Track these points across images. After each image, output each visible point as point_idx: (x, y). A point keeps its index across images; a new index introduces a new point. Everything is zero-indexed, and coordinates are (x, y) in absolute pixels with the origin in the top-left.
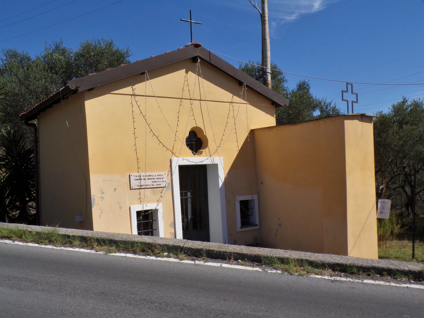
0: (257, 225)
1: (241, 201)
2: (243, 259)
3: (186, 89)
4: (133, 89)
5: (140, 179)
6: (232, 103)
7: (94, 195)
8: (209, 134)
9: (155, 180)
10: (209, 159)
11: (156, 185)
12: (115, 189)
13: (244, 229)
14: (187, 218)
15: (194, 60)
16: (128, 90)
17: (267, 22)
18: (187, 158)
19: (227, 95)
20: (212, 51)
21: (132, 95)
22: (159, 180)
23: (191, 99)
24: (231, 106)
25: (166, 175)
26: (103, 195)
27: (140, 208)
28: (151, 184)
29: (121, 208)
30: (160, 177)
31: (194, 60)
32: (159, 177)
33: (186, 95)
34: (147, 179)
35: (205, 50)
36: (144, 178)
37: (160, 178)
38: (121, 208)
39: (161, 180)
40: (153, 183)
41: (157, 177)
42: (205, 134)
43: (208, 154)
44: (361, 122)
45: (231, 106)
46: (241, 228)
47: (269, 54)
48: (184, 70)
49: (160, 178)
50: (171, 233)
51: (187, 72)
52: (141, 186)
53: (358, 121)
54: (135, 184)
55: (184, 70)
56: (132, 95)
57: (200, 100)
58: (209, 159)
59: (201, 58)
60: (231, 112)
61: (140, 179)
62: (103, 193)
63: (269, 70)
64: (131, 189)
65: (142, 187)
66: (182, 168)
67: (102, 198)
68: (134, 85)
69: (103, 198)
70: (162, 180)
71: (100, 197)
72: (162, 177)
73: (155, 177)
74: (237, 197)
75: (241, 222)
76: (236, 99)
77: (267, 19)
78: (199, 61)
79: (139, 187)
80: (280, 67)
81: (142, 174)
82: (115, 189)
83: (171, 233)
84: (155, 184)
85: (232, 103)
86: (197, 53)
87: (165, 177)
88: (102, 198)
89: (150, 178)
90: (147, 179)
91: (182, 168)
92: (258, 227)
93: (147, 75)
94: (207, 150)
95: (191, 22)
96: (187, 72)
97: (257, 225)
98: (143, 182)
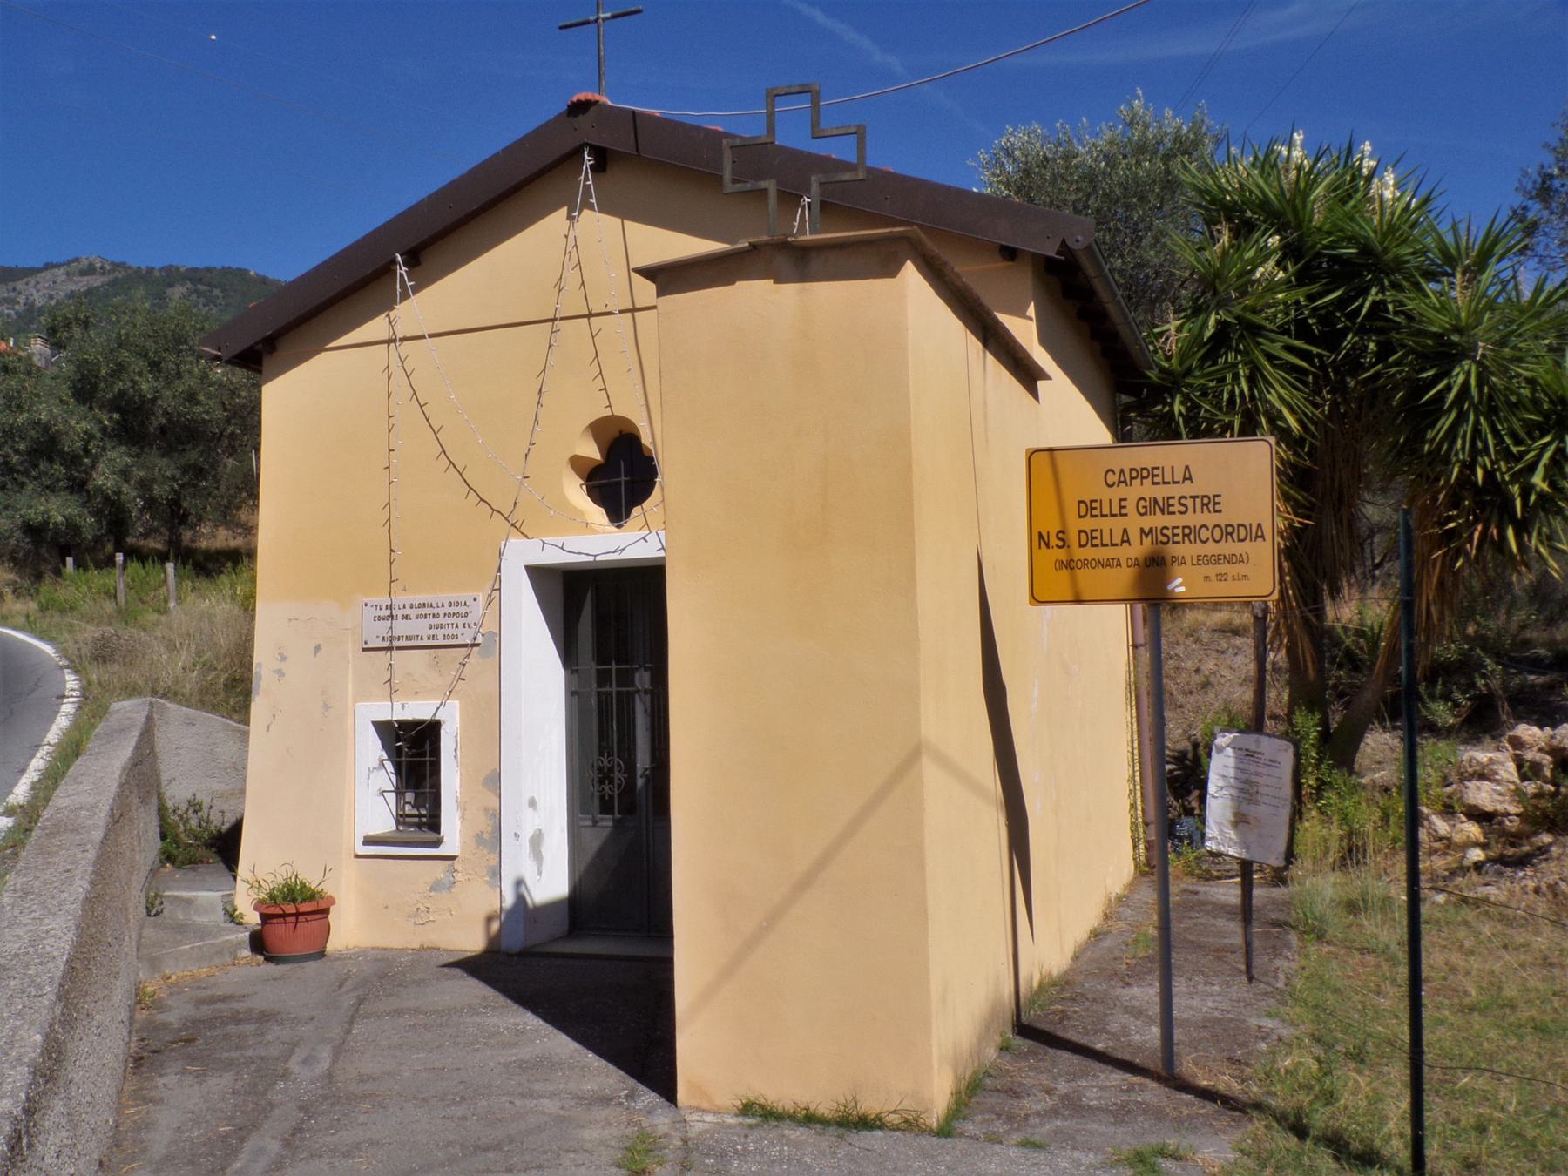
3: (572, 279)
7: (259, 665)
10: (652, 538)
12: (318, 648)
14: (630, 768)
16: (375, 328)
18: (558, 541)
21: (388, 342)
22: (454, 620)
23: (590, 315)
26: (283, 666)
29: (327, 707)
30: (458, 611)
32: (454, 610)
33: (573, 303)
36: (405, 612)
38: (327, 707)
39: (460, 621)
41: (447, 610)
50: (486, 810)
52: (392, 639)
54: (376, 632)
56: (388, 342)
58: (652, 538)
62: (284, 658)
65: (396, 644)
67: (280, 673)
72: (462, 610)
73: (441, 611)
79: (386, 644)
81: (399, 599)
82: (318, 648)
84: (440, 633)
88: (280, 673)
89: (423, 610)
98: (401, 628)
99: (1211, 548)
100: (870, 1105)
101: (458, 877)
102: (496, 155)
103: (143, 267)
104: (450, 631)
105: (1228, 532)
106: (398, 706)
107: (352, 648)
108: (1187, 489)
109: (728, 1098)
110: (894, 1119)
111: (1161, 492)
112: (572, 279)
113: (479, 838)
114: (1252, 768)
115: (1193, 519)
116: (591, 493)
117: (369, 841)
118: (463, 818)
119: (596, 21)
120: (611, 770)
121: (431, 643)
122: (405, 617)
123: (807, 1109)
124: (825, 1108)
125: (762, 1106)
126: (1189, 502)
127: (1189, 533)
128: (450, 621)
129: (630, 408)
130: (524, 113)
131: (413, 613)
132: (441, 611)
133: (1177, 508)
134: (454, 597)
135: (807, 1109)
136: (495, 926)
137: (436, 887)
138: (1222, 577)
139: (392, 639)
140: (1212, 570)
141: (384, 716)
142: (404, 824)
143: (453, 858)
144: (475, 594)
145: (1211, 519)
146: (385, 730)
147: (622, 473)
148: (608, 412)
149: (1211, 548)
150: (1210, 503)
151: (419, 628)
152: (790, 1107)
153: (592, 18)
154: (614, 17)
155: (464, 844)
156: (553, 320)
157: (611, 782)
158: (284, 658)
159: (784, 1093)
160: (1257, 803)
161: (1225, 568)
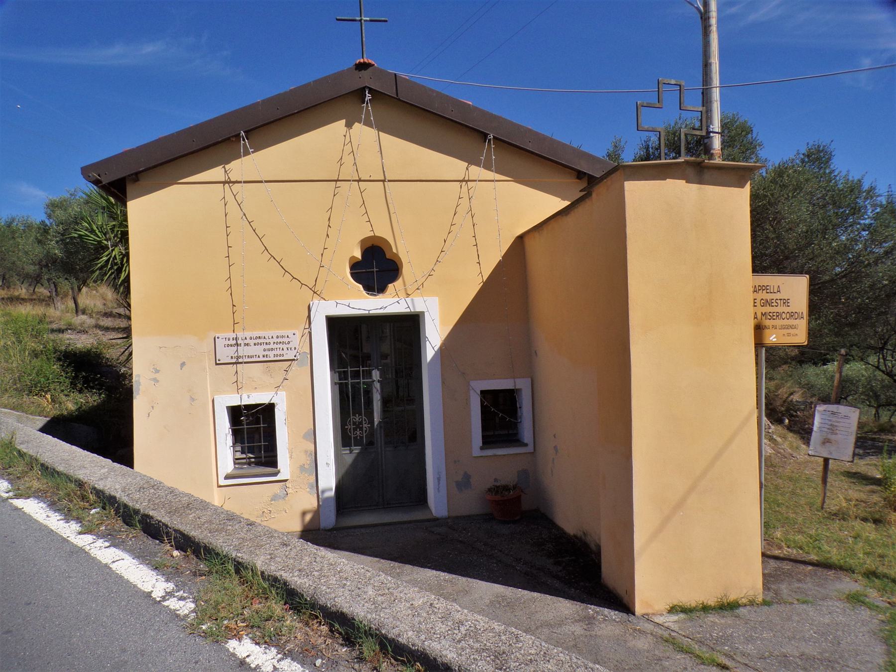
0: (526, 445)
1: (483, 393)
2: (858, 478)
3: (348, 160)
4: (226, 171)
5: (237, 344)
6: (467, 181)
7: (138, 376)
8: (403, 249)
9: (271, 346)
10: (402, 302)
11: (261, 356)
12: (183, 364)
13: (489, 452)
14: (371, 421)
15: (359, 94)
16: (216, 173)
17: (714, 28)
18: (346, 302)
19: (455, 167)
20: (403, 74)
21: (224, 183)
22: (281, 346)
23: (359, 181)
24: (465, 188)
25: (298, 335)
26: (157, 376)
27: (235, 401)
28: (262, 353)
29: (193, 399)
30: (282, 341)
31: (359, 94)
32: (279, 340)
33: (348, 172)
34: (252, 344)
35: (382, 73)
36: (246, 342)
37: (283, 343)
38: (193, 399)
39: (285, 346)
40: (265, 353)
41: (275, 340)
42: (394, 251)
43: (402, 294)
44: (695, 187)
45: (465, 188)
46: (482, 448)
47: (716, 94)
48: (344, 121)
49: (283, 343)
50: (306, 452)
51: (349, 125)
52: (238, 357)
53: (682, 182)
54: (225, 354)
55: (344, 121)
56: (224, 183)
57: (384, 181)
58: (402, 302)
59: (371, 91)
60: (465, 202)
61: (237, 344)
62: (157, 371)
63: (716, 126)
64: (217, 364)
65: (240, 360)
66: (334, 323)
67: (156, 380)
68: (228, 162)
69: (158, 381)
70: (287, 346)
71: (151, 379)
72: (286, 340)
73: (272, 341)
74: (473, 384)
75: (483, 437)
76: (477, 172)
77: (713, 21)
78: (368, 97)
79: (234, 361)
80: (746, 117)
81: (240, 335)
82: (183, 364)
83: (306, 452)
84: (271, 354)
85: (467, 181)
86: (366, 79)
87: (296, 341)
88: (156, 380)
89: (259, 341)
90: (252, 344)
91: (334, 323)
92: (530, 449)
93: (244, 140)
94: (398, 283)
95: (360, 20)
96: (349, 125)
97: (526, 445)
98: (243, 351)
99: (786, 322)
100: (732, 597)
101: (289, 491)
102: (308, 85)
103: (637, 150)
104: (278, 352)
105: (792, 315)
106: (245, 396)
107: (209, 362)
108: (778, 296)
109: (662, 605)
110: (744, 601)
111: (769, 297)
112: (348, 160)
113: (302, 468)
114: (834, 419)
115: (780, 309)
116: (352, 275)
117: (227, 477)
118: (291, 457)
119: (360, 20)
120: (361, 423)
121: (265, 359)
122: (247, 345)
123: (703, 604)
124: (712, 602)
125: (680, 607)
126: (779, 301)
127: (779, 315)
128: (278, 346)
129: (383, 231)
130: (333, 61)
131: (252, 342)
132: (272, 341)
133: (775, 304)
134: (280, 333)
135: (703, 604)
136: (308, 517)
137: (275, 498)
138: (789, 334)
139: (238, 357)
140: (786, 331)
141: (236, 402)
142: (238, 464)
143: (286, 481)
144: (294, 331)
145: (786, 309)
146: (235, 413)
147: (376, 266)
148: (372, 234)
149: (786, 322)
150: (786, 302)
151: (258, 351)
152: (693, 604)
153: (358, 18)
154: (371, 21)
155: (292, 473)
156: (336, 181)
157: (361, 429)
158: (157, 371)
159: (691, 598)
160: (836, 434)
161: (790, 331)
